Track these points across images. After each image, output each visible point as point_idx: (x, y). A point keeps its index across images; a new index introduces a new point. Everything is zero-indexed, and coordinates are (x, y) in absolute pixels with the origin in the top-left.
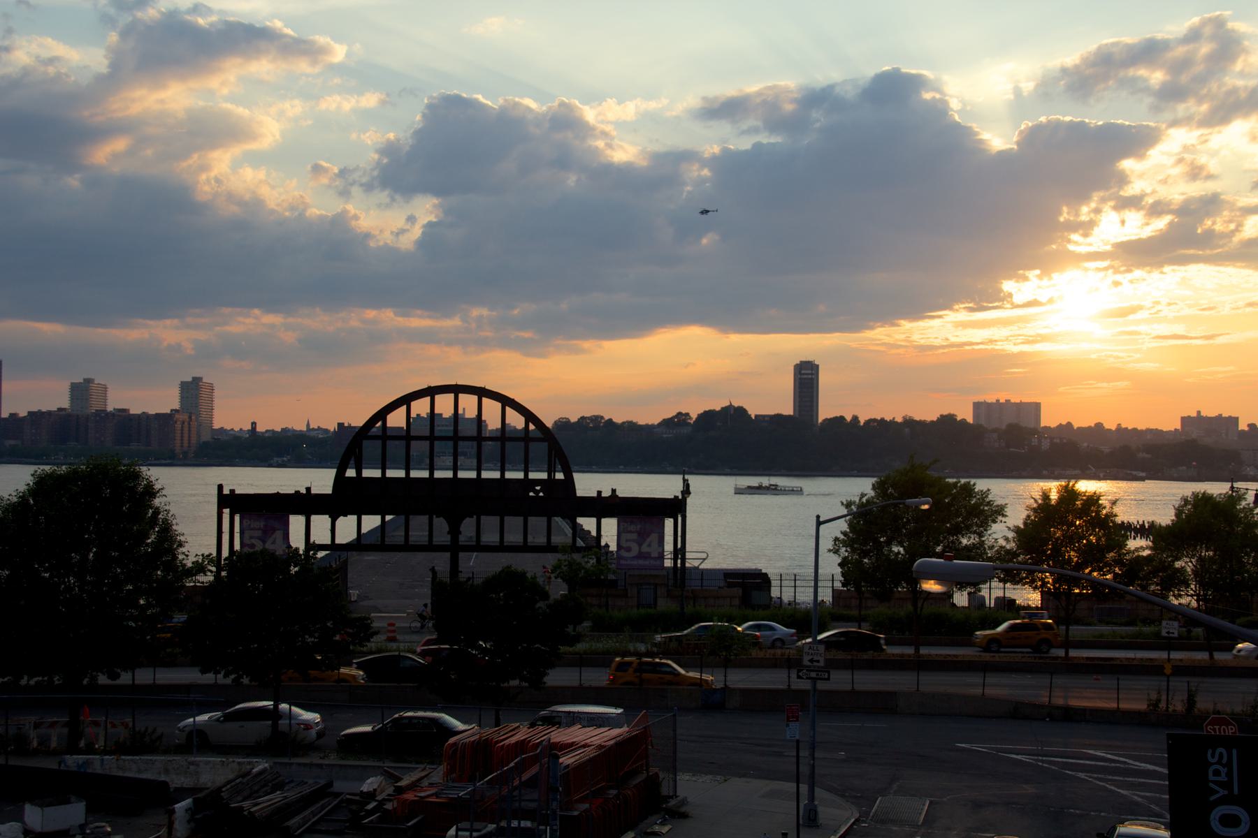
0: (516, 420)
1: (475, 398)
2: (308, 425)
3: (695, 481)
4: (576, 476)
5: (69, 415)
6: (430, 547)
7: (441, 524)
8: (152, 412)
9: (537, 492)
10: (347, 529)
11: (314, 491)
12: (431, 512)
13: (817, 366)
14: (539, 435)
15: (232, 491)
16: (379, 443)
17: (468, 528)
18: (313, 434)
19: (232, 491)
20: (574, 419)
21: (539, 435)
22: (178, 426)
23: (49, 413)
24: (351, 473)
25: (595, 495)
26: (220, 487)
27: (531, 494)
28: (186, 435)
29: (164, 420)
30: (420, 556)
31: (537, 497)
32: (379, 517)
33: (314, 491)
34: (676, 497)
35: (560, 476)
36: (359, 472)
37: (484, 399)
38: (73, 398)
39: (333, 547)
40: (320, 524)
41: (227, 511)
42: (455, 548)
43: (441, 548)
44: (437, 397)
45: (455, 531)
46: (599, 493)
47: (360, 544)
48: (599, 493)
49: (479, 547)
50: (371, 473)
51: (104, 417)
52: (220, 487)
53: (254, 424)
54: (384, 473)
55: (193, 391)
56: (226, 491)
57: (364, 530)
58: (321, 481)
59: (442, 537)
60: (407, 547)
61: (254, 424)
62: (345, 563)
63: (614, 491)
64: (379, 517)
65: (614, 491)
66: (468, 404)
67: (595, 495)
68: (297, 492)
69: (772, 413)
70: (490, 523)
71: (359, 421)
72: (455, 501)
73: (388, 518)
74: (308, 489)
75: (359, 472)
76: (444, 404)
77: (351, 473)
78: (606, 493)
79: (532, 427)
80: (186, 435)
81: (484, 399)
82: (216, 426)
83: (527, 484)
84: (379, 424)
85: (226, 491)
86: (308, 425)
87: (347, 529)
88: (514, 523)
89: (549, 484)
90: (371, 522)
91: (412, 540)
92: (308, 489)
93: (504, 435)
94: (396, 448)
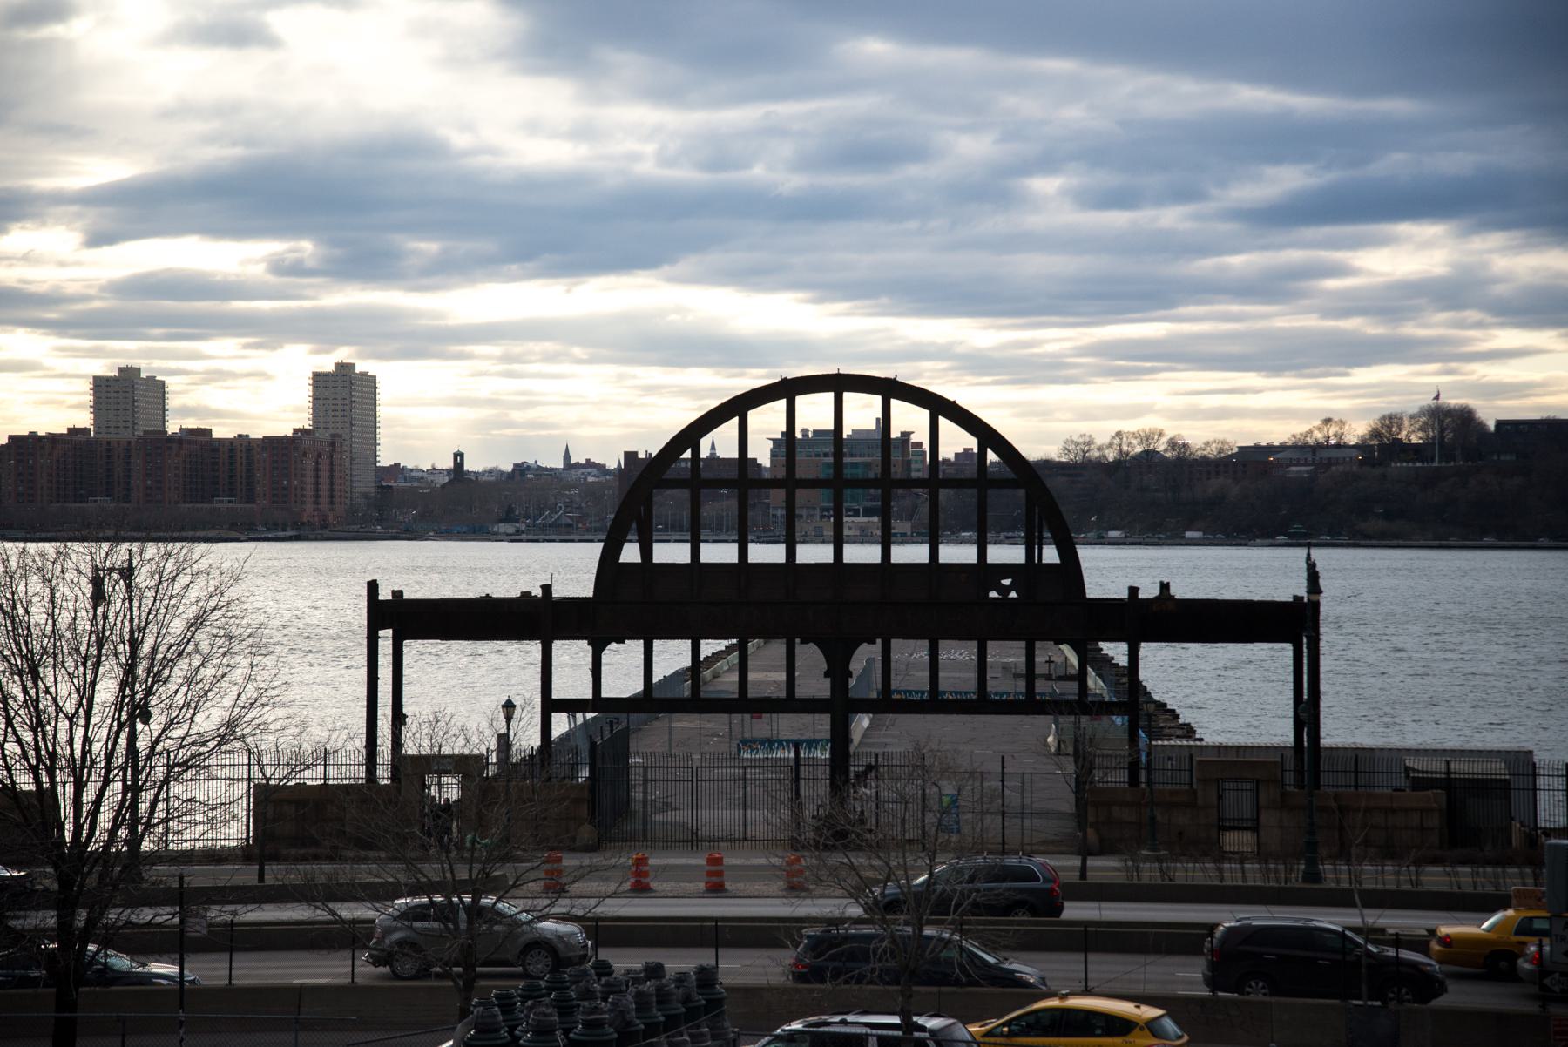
0: (955, 441)
1: (877, 400)
2: (567, 456)
3: (1332, 561)
4: (1085, 553)
5: (91, 443)
6: (790, 703)
7: (810, 657)
8: (257, 434)
9: (1004, 591)
10: (623, 671)
11: (557, 593)
12: (790, 632)
13: (374, 378)
14: (1009, 474)
15: (398, 594)
16: (684, 494)
17: (865, 656)
18: (575, 474)
19: (398, 594)
20: (508, 467)
21: (1009, 474)
22: (309, 462)
23: (52, 438)
24: (630, 553)
25: (1125, 595)
26: (373, 587)
27: (993, 594)
28: (324, 479)
29: (278, 452)
30: (717, 723)
31: (1004, 601)
32: (686, 645)
33: (557, 593)
34: (1297, 599)
35: (1050, 555)
36: (647, 552)
37: (894, 403)
38: (98, 408)
39: (597, 702)
40: (572, 657)
41: (386, 635)
42: (841, 706)
43: (812, 706)
44: (802, 401)
45: (838, 671)
46: (1133, 591)
47: (652, 701)
48: (1133, 591)
49: (887, 703)
50: (672, 552)
51: (161, 443)
52: (373, 587)
53: (459, 456)
54: (791, 553)
55: (343, 395)
56: (385, 594)
57: (657, 676)
58: (570, 568)
59: (814, 685)
60: (744, 703)
61: (459, 456)
62: (625, 735)
63: (1165, 587)
64: (686, 645)
65: (1165, 587)
66: (862, 412)
67: (1125, 595)
68: (526, 595)
69: (1251, 444)
70: (910, 655)
71: (651, 446)
72: (833, 611)
73: (709, 647)
74: (547, 589)
75: (647, 552)
76: (815, 412)
77: (630, 553)
78: (1149, 591)
79: (992, 456)
80: (324, 479)
81: (894, 403)
82: (385, 460)
83: (984, 572)
84: (687, 454)
85: (385, 594)
86: (567, 456)
87: (623, 671)
88: (958, 655)
89: (1028, 572)
90: (672, 656)
91: (802, 691)
92: (547, 589)
93: (938, 476)
94: (722, 505)
